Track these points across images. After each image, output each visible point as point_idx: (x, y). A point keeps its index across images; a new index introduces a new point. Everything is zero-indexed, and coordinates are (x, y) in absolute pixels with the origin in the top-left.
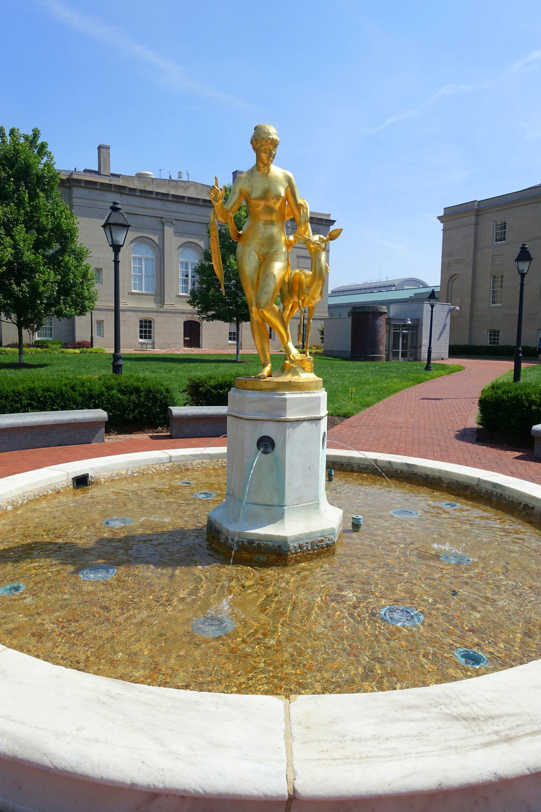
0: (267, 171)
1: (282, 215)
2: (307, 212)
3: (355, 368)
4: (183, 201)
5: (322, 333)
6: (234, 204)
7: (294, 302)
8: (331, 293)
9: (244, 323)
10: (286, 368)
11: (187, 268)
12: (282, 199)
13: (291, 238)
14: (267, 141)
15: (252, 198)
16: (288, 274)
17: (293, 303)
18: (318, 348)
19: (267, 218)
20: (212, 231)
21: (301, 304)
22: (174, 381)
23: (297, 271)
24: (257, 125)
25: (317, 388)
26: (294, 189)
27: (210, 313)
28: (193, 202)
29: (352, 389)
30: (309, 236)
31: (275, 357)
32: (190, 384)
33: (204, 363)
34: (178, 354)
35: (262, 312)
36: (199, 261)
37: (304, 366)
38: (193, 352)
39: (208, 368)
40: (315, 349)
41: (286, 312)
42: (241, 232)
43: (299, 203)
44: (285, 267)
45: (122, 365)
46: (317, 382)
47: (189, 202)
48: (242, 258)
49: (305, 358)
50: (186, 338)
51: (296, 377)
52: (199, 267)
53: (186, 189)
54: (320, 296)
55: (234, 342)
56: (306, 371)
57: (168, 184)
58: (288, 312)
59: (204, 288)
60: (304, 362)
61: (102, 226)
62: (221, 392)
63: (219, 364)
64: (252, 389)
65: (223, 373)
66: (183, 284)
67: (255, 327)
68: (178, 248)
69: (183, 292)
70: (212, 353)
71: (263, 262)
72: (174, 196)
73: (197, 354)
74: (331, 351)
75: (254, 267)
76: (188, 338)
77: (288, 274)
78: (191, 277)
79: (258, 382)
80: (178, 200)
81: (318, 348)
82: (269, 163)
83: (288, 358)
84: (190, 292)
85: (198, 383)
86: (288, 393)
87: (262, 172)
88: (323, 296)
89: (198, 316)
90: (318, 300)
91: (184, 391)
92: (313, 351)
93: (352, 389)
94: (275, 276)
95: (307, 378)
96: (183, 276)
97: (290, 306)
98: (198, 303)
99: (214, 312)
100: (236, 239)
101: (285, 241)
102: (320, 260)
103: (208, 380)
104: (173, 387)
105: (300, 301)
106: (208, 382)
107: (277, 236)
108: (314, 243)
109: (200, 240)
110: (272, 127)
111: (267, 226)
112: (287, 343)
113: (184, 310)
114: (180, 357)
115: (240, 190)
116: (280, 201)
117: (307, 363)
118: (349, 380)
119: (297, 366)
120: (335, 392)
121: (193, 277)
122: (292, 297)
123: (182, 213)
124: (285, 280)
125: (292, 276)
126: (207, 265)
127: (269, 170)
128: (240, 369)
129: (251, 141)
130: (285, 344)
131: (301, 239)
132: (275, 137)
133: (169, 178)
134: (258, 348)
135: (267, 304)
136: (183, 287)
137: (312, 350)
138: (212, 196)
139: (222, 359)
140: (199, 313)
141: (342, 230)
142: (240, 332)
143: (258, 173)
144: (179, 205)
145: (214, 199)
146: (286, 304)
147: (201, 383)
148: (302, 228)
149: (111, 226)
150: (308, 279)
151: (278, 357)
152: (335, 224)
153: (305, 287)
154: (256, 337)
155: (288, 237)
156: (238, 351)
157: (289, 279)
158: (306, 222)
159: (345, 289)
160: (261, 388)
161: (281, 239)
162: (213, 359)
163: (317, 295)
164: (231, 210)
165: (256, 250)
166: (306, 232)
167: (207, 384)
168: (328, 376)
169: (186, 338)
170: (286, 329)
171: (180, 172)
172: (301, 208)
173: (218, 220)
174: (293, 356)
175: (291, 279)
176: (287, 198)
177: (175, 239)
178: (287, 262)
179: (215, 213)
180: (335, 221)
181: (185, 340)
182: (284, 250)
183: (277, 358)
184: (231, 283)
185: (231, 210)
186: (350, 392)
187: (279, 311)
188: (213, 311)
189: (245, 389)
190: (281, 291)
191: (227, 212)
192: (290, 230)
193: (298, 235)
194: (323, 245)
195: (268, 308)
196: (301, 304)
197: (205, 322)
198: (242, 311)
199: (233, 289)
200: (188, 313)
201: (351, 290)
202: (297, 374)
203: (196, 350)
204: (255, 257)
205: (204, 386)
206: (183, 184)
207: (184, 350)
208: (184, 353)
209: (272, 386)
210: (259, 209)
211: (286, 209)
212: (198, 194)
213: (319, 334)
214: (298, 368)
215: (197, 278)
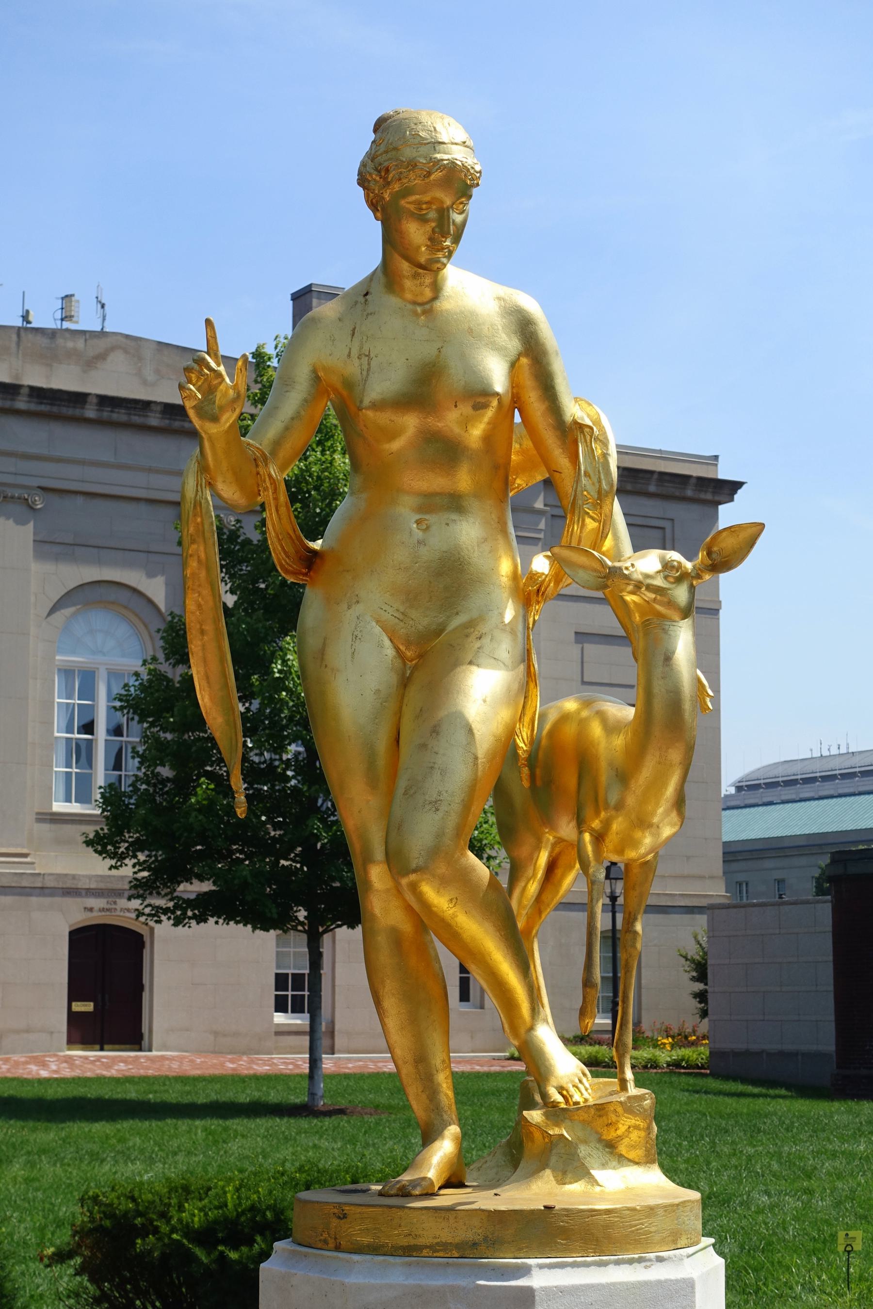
0: (428, 293)
1: (496, 467)
2: (605, 456)
3: (858, 1133)
4: (77, 412)
5: (701, 971)
6: (287, 428)
7: (559, 841)
8: (732, 790)
9: (343, 933)
10: (528, 1145)
11: (88, 691)
12: (495, 403)
13: (541, 564)
14: (429, 174)
15: (366, 402)
16: (527, 719)
17: (554, 845)
18: (682, 1040)
19: (435, 482)
20: (193, 541)
21: (589, 848)
22: (17, 1208)
23: (570, 705)
24: (388, 110)
25: (674, 1239)
26: (548, 364)
27: (191, 889)
28: (120, 416)
29: (851, 1234)
30: (618, 557)
31: (489, 1085)
32: (92, 1219)
33: (159, 1118)
34: (42, 1081)
35: (414, 887)
36: (145, 663)
37: (611, 1135)
38: (108, 1067)
39: (175, 1143)
40: (673, 1046)
41: (524, 889)
42: (317, 545)
43: (568, 418)
44: (516, 686)
46: (672, 1209)
47: (105, 415)
48: (322, 652)
49: (614, 1098)
50: (78, 1007)
51: (577, 1187)
52: (143, 688)
53: (91, 363)
54: (674, 815)
55: (300, 1021)
56: (622, 1160)
57: (13, 346)
58: (533, 888)
59: (164, 781)
60: (613, 1118)
62: (233, 1255)
63: (229, 1123)
64: (374, 1250)
65: (246, 1164)
66: (68, 765)
67: (385, 957)
68: (53, 610)
69: (68, 800)
70: (197, 1072)
71: (415, 668)
72: (37, 393)
73: (129, 1080)
74: (747, 1053)
75: (378, 691)
76: (87, 1007)
77: (527, 719)
78: (109, 732)
79: (400, 1213)
80: (55, 409)
81: (682, 1040)
82: (438, 261)
83: (538, 1098)
84: (103, 795)
85: (126, 1213)
86: (541, 1267)
87: (409, 296)
88: (688, 811)
89: (136, 904)
90: (667, 831)
91: (61, 1257)
92: (664, 1056)
93: (851, 1234)
94: (470, 731)
95: (627, 1188)
96: (69, 730)
97: (543, 858)
98: (137, 846)
99: (207, 886)
100: (295, 573)
101: (515, 577)
102: (668, 658)
103: (174, 1201)
104: (11, 1235)
105: (587, 837)
106: (173, 1212)
107: (477, 557)
108: (638, 586)
109: (151, 575)
110: (448, 119)
111: (432, 518)
112: (532, 1028)
113: (74, 877)
114: (51, 1093)
115: (315, 371)
116: (490, 413)
117: (625, 1123)
118: (834, 1189)
119: (580, 1134)
120: (769, 1248)
121: (117, 731)
122: (548, 820)
123: (82, 463)
124: (515, 746)
125: (547, 727)
126: (178, 678)
127: (437, 289)
128: (324, 1144)
129: (360, 173)
130: (522, 1031)
131: (583, 567)
132: (459, 155)
133: (18, 322)
134: (398, 1052)
135: (435, 852)
136: (68, 775)
137: (658, 1053)
138: (192, 396)
139: (243, 1098)
140: (140, 889)
141: (759, 528)
142: (325, 971)
143: (393, 301)
144: (58, 430)
145: (198, 409)
146: (523, 851)
147: (139, 1214)
148: (588, 521)
150: (619, 742)
151: (501, 1085)
152: (744, 486)
153: (604, 776)
154: (390, 1003)
155: (527, 561)
156: (314, 1063)
157: (535, 742)
158: (601, 497)
159: (796, 771)
160: (412, 1242)
161: (495, 570)
162: (201, 1100)
163: (660, 810)
164: (274, 452)
165: (386, 616)
166: (604, 537)
167: (168, 1221)
168: (733, 1172)
169: (78, 1007)
170: (524, 966)
171: (67, 298)
172: (580, 437)
173: (216, 494)
174: (561, 1089)
175: (544, 742)
176: (516, 401)
177: (37, 568)
178: (522, 667)
179: (203, 468)
180: (736, 486)
181: (73, 1018)
182: (509, 613)
183: (496, 1093)
184: (285, 757)
185: (274, 452)
186: (841, 1249)
187: (493, 883)
188: (201, 878)
189: (338, 1248)
190: (500, 791)
191: (259, 460)
192: (542, 525)
193: (566, 553)
194: (681, 594)
195: (442, 869)
196: (589, 848)
197: (164, 929)
198: (334, 879)
199: (293, 782)
200: (90, 892)
201: (826, 779)
202: (583, 1173)
203: (124, 1061)
204: (381, 646)
205: (156, 1231)
206: (80, 344)
207: (69, 1060)
208: (67, 1073)
209: (463, 1234)
210: (396, 445)
211: (516, 446)
212: (145, 382)
213: (687, 976)
214: (585, 1142)
215: (133, 737)
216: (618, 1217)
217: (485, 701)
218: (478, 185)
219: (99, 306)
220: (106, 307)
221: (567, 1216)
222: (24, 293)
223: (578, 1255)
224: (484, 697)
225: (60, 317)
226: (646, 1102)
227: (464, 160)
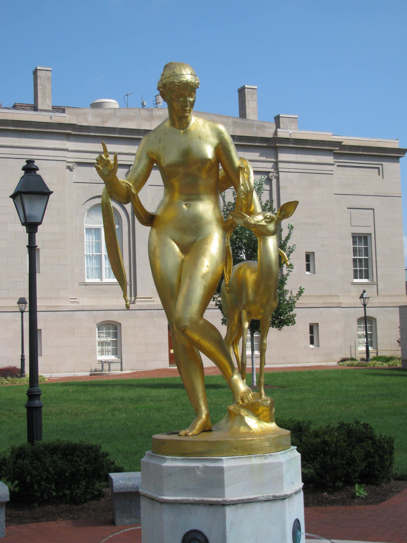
45: (41, 407)
61: (11, 197)
149: (22, 195)
217: (208, 266)
218: (198, 87)
221: (236, 442)
224: (207, 265)
225: (155, 103)
226: (268, 402)
227: (191, 80)
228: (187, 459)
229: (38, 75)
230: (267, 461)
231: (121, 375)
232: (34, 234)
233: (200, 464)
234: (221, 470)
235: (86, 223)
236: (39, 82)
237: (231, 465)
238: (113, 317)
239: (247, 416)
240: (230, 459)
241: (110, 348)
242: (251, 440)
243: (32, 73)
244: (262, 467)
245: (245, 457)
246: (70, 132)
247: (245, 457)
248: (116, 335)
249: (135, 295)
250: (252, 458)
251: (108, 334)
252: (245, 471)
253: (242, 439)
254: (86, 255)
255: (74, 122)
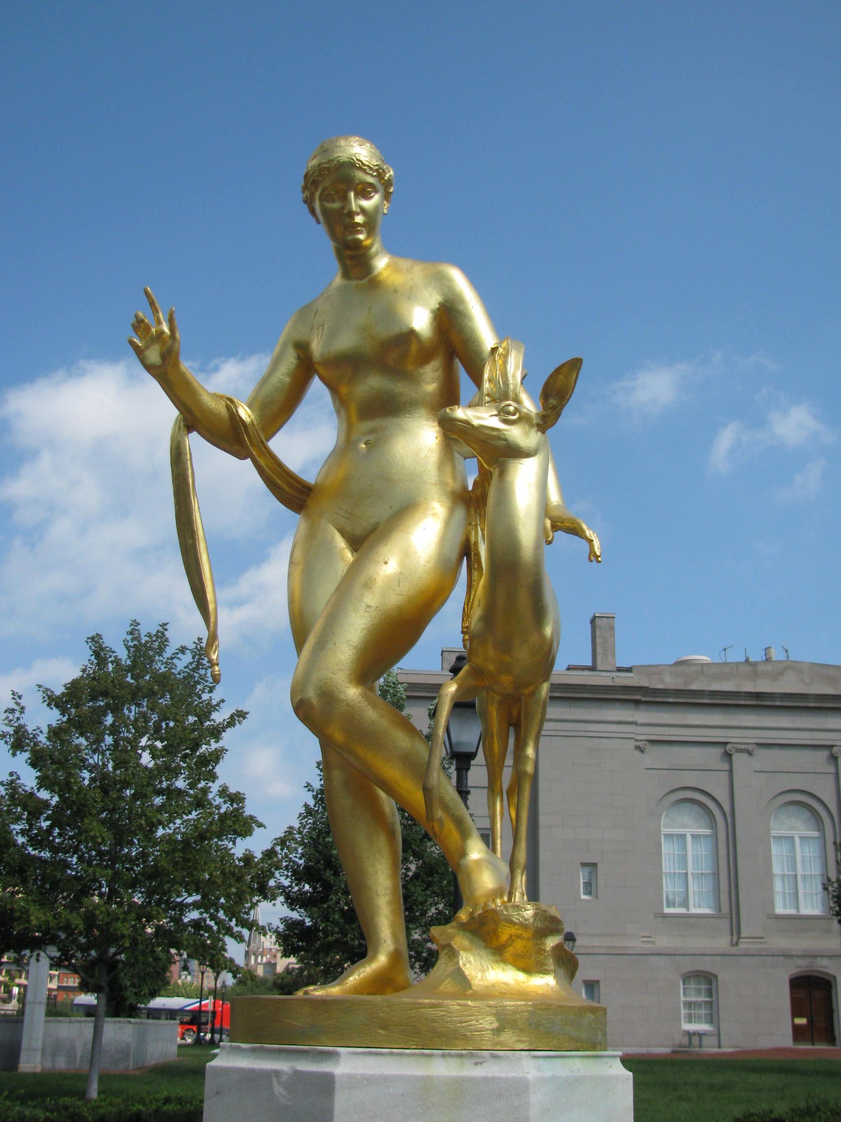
76: (802, 1021)
216: (445, 1011)
219: (784, 651)
220: (788, 651)
222: (745, 649)
223: (398, 1046)
228: (262, 1049)
229: (597, 624)
230: (478, 1072)
231: (718, 1054)
232: (464, 772)
233: (283, 1066)
234: (327, 1083)
235: (665, 826)
236: (598, 633)
237: (360, 1072)
238: (706, 965)
239: (465, 949)
240: (362, 1053)
241: (703, 1012)
242: (433, 1006)
243: (589, 622)
244: (459, 1086)
245: (411, 1055)
246: (638, 697)
247: (411, 1055)
248: (710, 993)
249: (739, 933)
250: (433, 1059)
251: (698, 992)
252: (403, 1095)
253: (405, 1000)
254: (666, 873)
255: (644, 683)
